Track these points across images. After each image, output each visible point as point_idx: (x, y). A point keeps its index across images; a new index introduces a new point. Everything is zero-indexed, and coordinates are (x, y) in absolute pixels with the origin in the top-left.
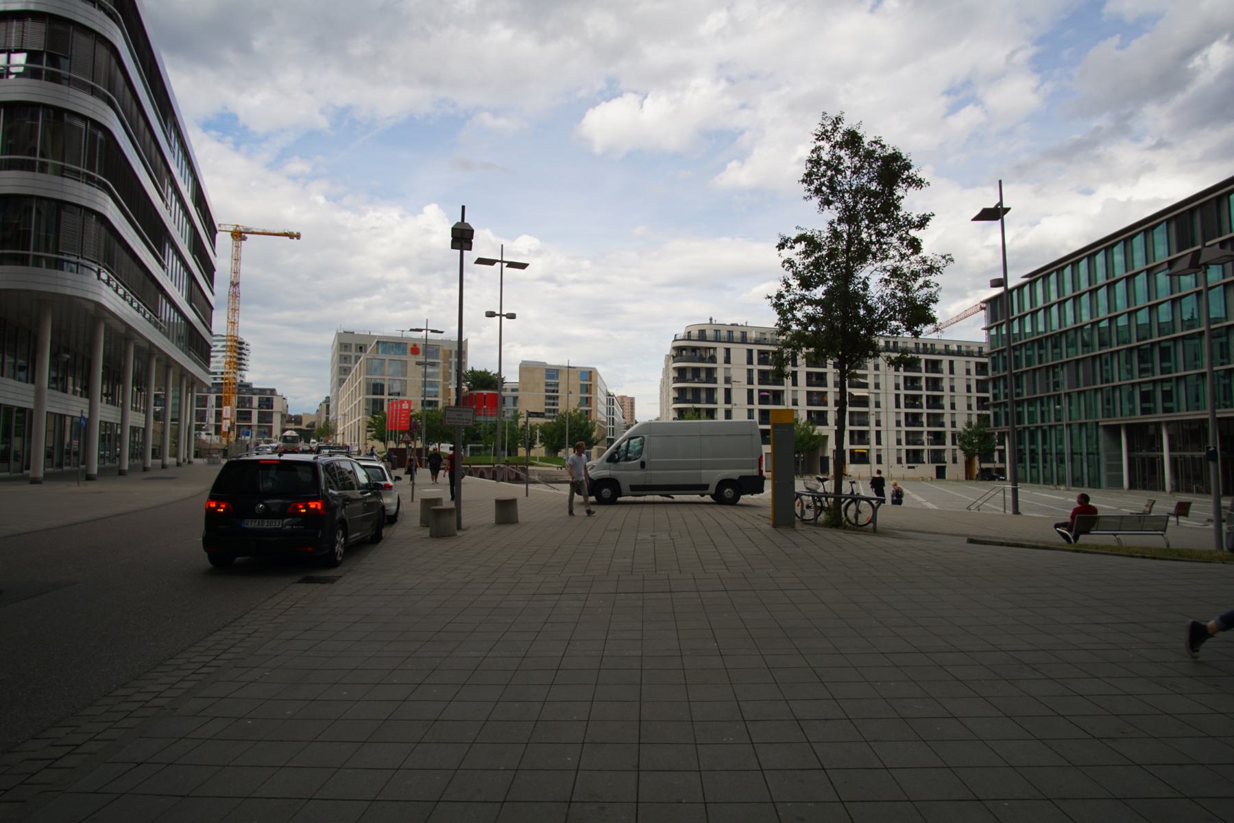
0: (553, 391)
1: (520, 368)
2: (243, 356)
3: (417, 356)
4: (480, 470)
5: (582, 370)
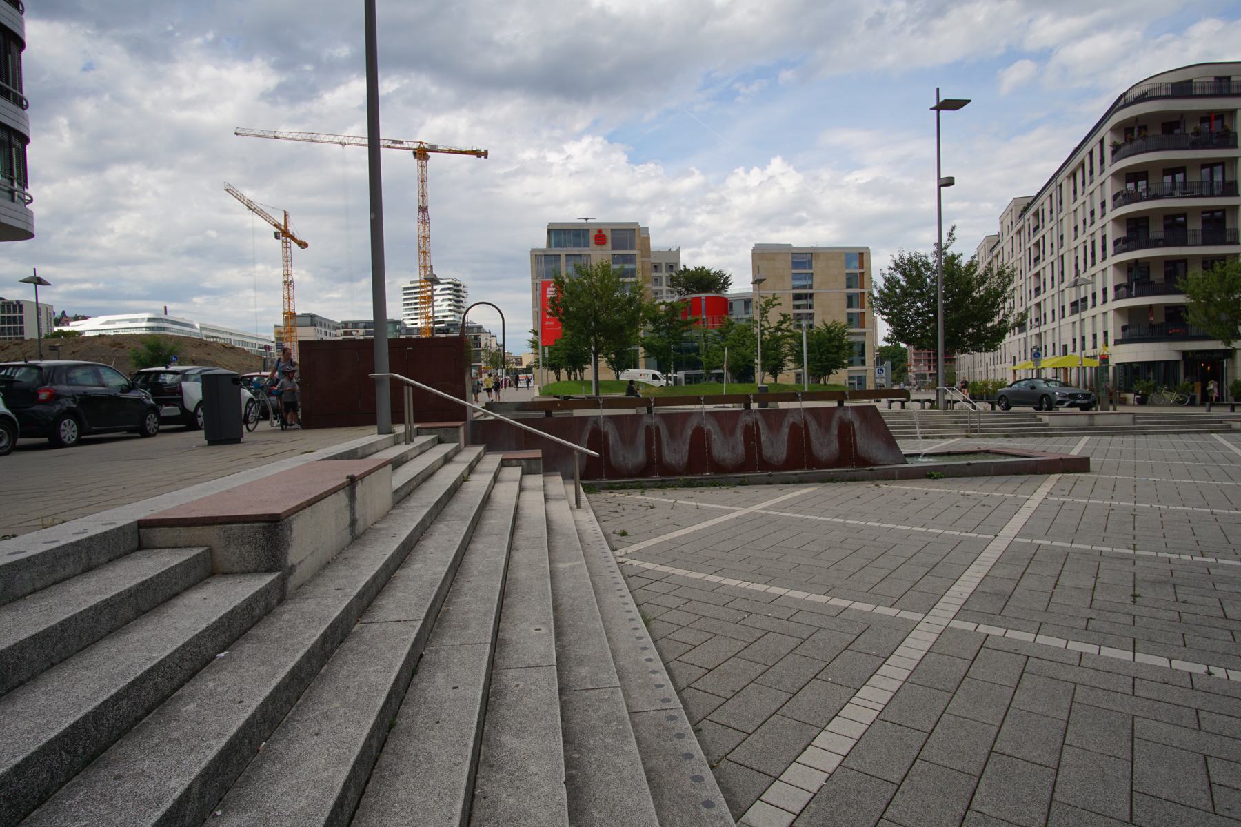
0: (804, 287)
1: (753, 254)
2: (461, 299)
3: (604, 247)
4: (694, 423)
5: (847, 251)
